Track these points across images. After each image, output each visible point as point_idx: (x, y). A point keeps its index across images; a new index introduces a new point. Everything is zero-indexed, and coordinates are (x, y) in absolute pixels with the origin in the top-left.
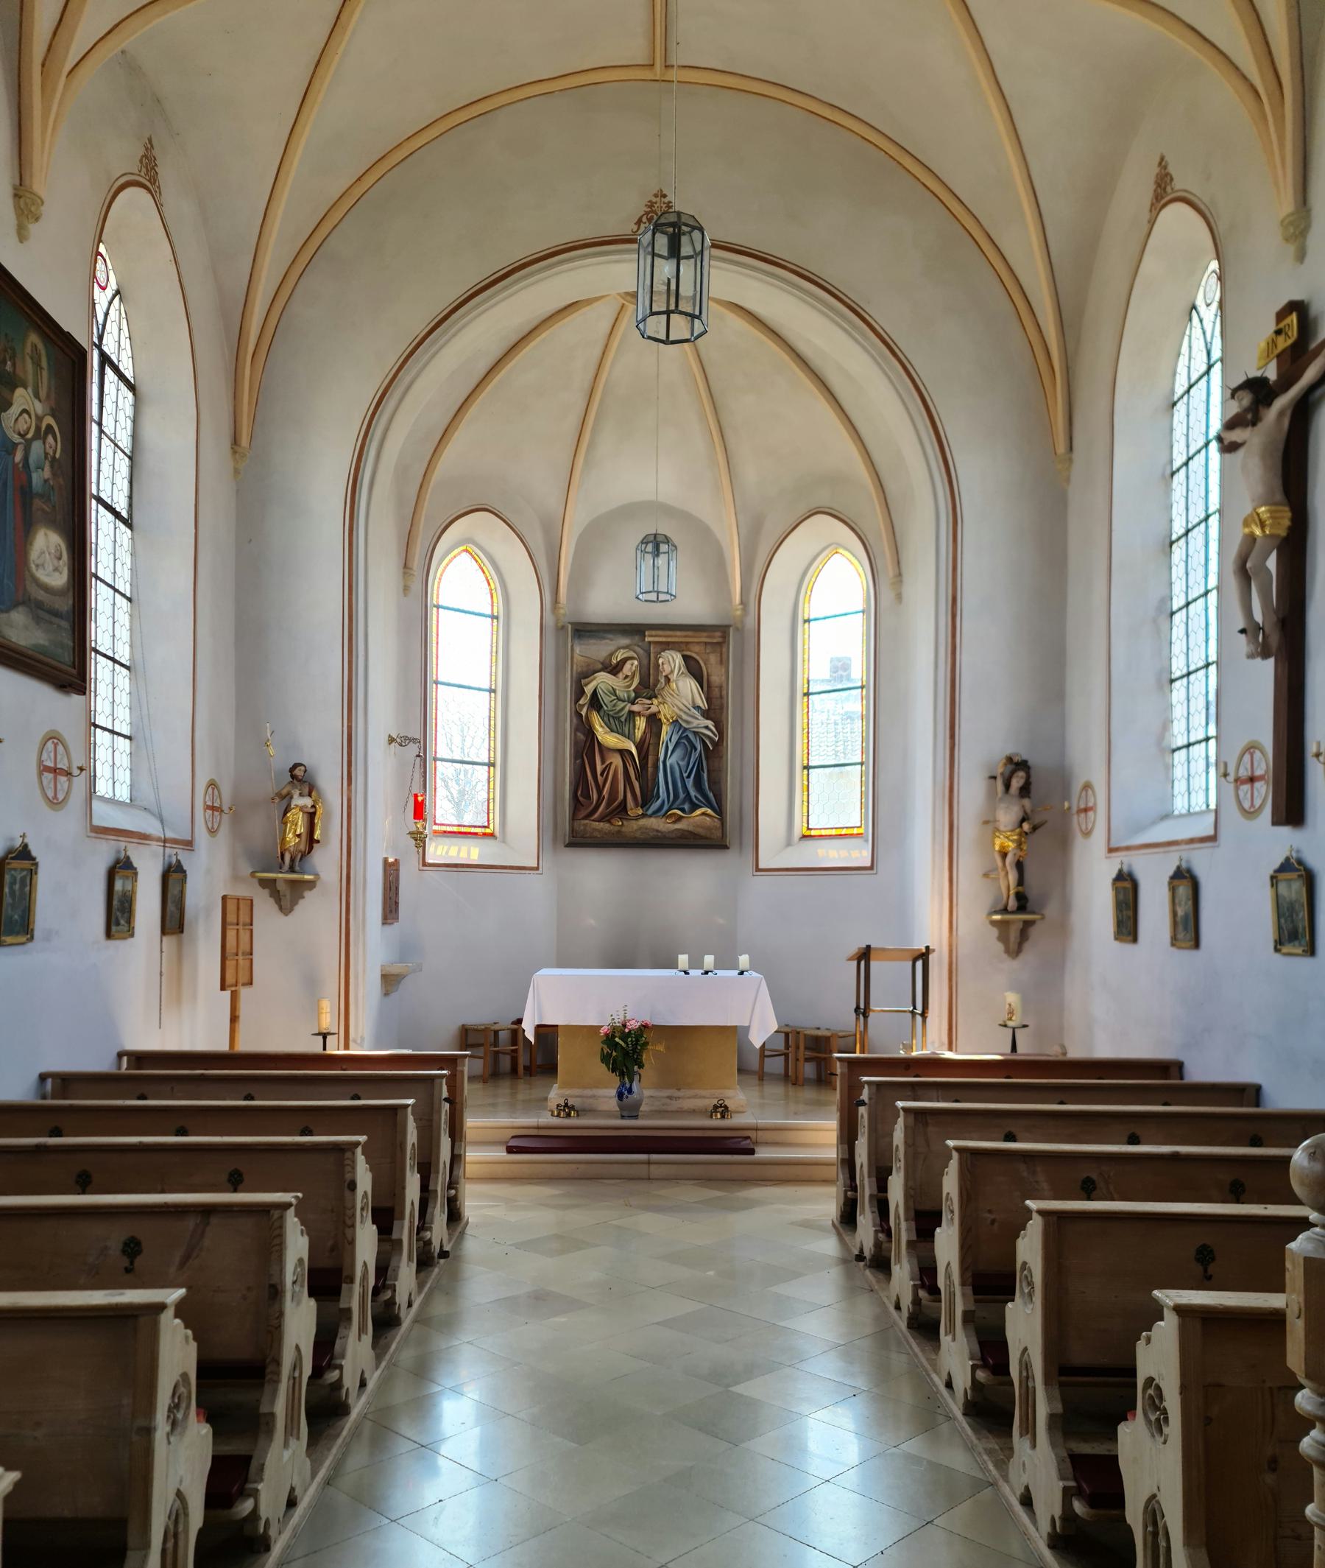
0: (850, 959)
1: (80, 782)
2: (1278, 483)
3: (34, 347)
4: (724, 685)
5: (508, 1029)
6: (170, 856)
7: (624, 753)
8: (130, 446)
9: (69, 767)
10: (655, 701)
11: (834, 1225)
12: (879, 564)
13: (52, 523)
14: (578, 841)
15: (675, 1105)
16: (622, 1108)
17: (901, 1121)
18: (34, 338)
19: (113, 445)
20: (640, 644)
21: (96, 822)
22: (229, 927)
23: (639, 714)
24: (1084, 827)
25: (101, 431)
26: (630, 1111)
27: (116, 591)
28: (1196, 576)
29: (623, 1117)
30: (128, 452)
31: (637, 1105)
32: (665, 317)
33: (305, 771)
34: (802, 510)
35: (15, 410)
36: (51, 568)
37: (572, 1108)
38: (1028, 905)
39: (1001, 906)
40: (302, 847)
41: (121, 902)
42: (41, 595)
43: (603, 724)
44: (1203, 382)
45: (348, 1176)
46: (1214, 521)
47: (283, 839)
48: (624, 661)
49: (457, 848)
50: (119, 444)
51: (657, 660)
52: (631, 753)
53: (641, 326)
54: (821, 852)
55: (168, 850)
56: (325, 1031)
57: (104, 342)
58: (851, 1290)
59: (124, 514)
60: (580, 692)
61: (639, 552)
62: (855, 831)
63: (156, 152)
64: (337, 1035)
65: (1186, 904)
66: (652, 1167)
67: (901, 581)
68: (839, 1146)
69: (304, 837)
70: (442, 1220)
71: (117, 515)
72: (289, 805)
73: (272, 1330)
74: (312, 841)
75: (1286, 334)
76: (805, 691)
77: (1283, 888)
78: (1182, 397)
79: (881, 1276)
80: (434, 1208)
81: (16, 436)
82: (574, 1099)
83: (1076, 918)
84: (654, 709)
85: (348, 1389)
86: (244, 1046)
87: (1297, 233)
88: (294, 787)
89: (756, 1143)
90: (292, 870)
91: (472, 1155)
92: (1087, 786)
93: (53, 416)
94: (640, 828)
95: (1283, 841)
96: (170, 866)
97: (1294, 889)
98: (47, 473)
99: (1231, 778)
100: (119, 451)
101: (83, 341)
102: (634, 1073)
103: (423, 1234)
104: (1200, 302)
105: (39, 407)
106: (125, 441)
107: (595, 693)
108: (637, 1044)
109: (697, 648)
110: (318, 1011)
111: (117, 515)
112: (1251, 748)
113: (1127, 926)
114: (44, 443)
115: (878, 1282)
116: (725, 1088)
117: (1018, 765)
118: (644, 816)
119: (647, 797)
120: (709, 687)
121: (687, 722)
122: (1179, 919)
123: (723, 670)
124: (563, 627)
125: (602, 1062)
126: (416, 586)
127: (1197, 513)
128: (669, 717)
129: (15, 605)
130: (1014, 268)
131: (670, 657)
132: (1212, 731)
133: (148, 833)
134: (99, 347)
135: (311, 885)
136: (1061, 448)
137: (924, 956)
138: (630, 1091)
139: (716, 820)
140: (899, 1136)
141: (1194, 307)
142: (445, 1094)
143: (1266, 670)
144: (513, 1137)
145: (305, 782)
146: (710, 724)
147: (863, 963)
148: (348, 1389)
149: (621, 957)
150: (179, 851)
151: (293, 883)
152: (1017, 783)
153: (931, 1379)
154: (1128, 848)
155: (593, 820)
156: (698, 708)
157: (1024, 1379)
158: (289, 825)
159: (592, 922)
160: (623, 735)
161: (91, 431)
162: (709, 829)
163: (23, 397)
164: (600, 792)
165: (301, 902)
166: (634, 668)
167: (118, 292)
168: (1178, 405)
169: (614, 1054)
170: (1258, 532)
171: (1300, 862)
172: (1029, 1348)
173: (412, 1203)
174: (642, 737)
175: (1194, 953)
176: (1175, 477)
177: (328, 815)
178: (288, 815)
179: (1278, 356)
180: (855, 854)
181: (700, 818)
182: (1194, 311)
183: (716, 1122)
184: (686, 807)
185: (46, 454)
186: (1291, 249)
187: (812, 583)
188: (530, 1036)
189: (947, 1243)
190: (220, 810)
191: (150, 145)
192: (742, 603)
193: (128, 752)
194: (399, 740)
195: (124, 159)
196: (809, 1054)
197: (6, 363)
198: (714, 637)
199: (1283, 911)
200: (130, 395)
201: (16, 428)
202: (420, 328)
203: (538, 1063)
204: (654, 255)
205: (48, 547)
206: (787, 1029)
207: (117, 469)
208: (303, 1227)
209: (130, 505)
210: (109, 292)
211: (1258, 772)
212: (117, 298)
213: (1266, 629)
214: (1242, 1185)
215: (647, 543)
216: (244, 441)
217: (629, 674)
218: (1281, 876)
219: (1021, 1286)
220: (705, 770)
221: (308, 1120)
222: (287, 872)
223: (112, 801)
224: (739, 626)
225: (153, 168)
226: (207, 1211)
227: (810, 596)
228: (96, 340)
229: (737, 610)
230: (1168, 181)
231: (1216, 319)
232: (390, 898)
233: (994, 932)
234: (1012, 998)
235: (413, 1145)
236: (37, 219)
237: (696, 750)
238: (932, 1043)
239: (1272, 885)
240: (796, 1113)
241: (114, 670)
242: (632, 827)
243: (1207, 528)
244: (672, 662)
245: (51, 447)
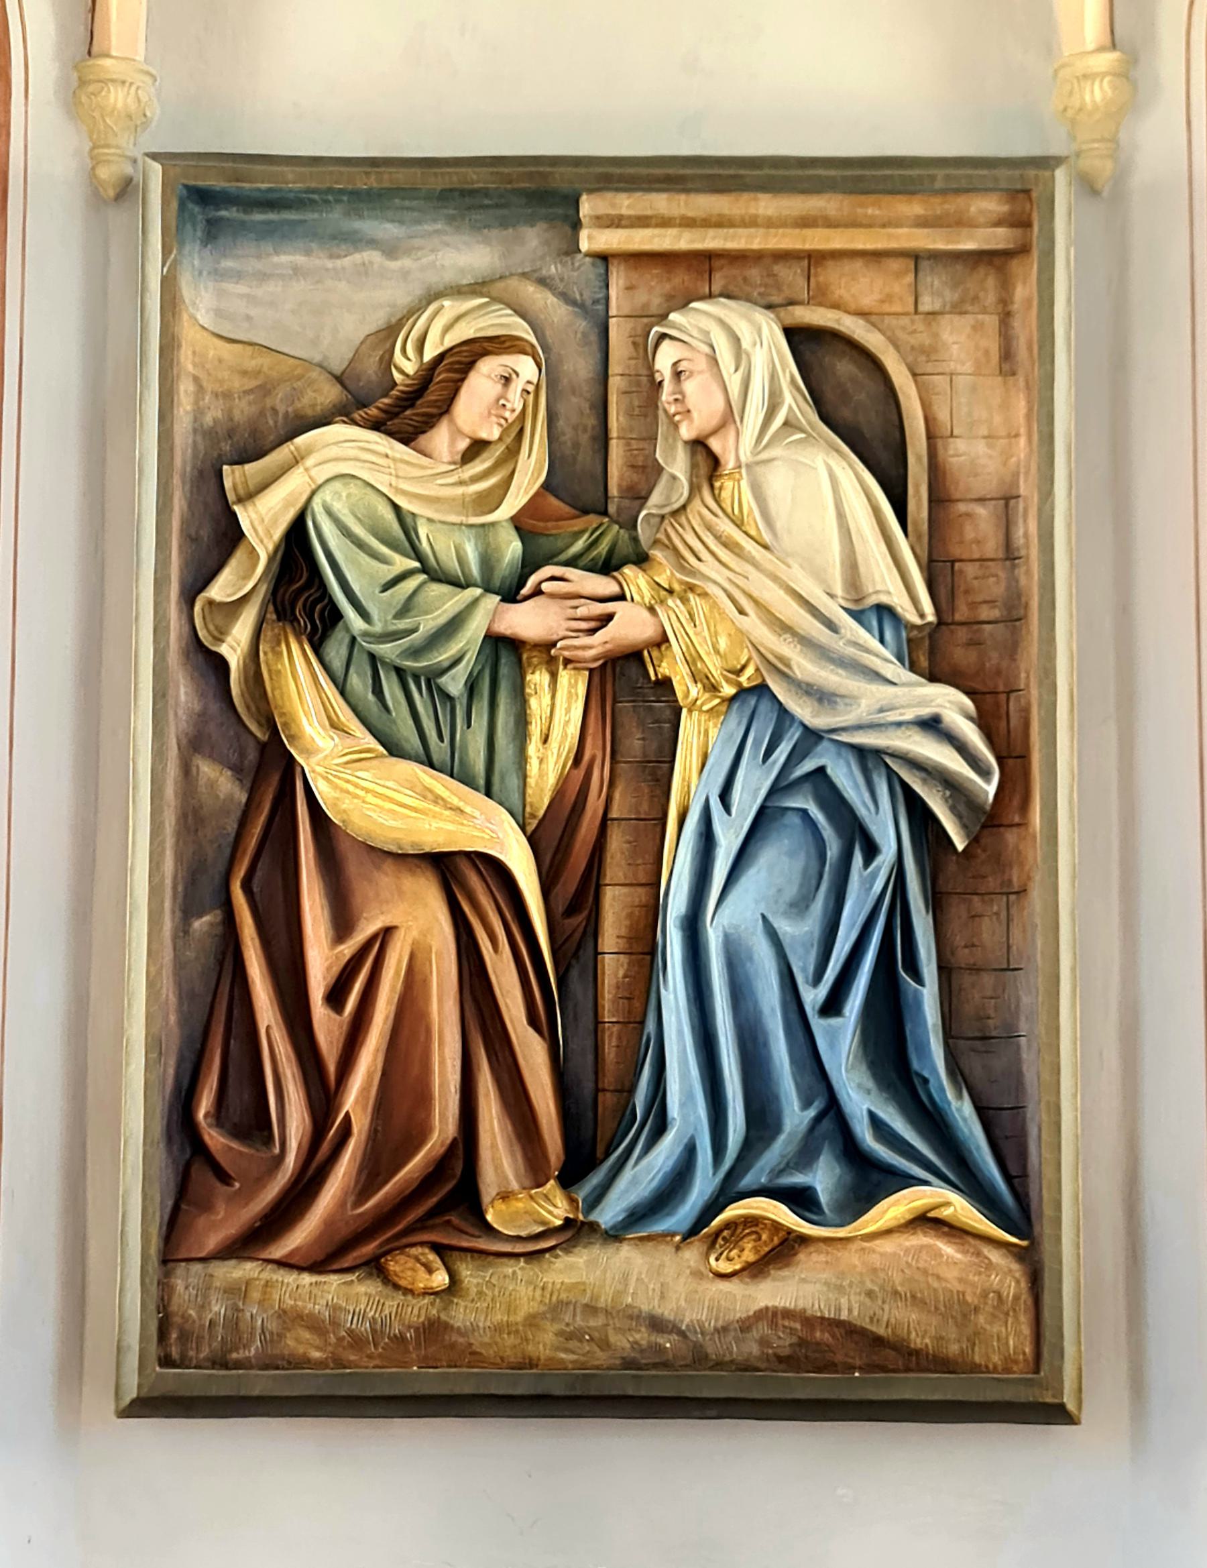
4: (1025, 488)
10: (635, 579)
51: (645, 351)
120: (939, 498)
121: (822, 697)
139: (995, 1256)
155: (282, 1264)
166: (515, 400)
177: (688, 623)
198: (960, 222)
217: (491, 432)
237: (871, 851)
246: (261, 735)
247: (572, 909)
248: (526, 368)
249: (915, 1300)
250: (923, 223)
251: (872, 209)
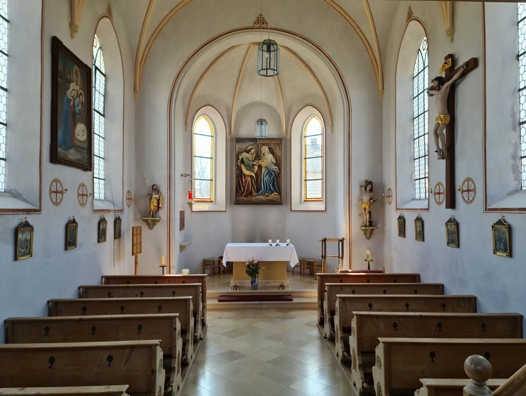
0: (320, 241)
1: (90, 198)
2: (446, 108)
3: (76, 70)
4: (281, 156)
5: (217, 260)
6: (116, 215)
7: (251, 177)
8: (104, 93)
9: (87, 193)
10: (260, 161)
11: (317, 325)
12: (327, 121)
13: (82, 122)
14: (238, 203)
15: (268, 285)
16: (252, 287)
17: (338, 300)
18: (76, 67)
19: (99, 93)
20: (256, 144)
21: (95, 208)
22: (134, 236)
23: (255, 165)
24: (389, 202)
25: (95, 90)
26: (255, 287)
27: (100, 136)
28: (421, 129)
29: (253, 289)
30: (103, 94)
31: (257, 286)
32: (266, 70)
33: (157, 187)
34: (304, 104)
35: (70, 90)
36: (81, 135)
37: (238, 287)
38: (372, 224)
39: (364, 225)
40: (156, 210)
41: (102, 232)
42: (78, 144)
43: (245, 168)
44: (422, 73)
45: (174, 327)
46: (426, 114)
47: (150, 207)
48: (251, 149)
49: (202, 206)
50: (101, 93)
51: (261, 149)
52: (253, 176)
53: (259, 72)
54: (310, 206)
55: (116, 214)
56: (163, 266)
57: (96, 63)
58: (323, 348)
59: (102, 113)
60: (238, 159)
61: (256, 124)
62: (320, 199)
63: (111, 6)
64: (166, 267)
65: (420, 228)
66: (262, 305)
67: (333, 126)
68: (318, 302)
69: (156, 207)
70: (200, 328)
71: (100, 114)
72: (152, 197)
73: (152, 383)
74: (159, 208)
75: (448, 64)
76: (305, 157)
77: (449, 227)
78: (416, 76)
79: (332, 344)
80: (198, 325)
81: (71, 97)
82: (238, 284)
83: (387, 228)
84: (260, 163)
85: (174, 392)
86: (140, 273)
87: (451, 34)
88: (153, 192)
89: (293, 297)
90: (153, 217)
91: (209, 302)
92: (390, 189)
93: (82, 90)
94: (256, 199)
95: (449, 213)
96: (116, 218)
97: (453, 228)
98: (80, 107)
99: (433, 193)
100: (101, 95)
101: (90, 65)
102: (256, 276)
103: (195, 334)
104: (421, 49)
105: (78, 88)
106: (102, 92)
107: (242, 159)
108: (257, 267)
109: (272, 145)
110: (161, 260)
111: (100, 114)
112: (439, 184)
113: (402, 232)
114: (79, 98)
115: (331, 346)
116: (283, 279)
117: (369, 183)
118: (257, 195)
119: (258, 190)
120: (276, 156)
121: (270, 167)
122: (418, 232)
123: (280, 152)
124: (232, 139)
125: (246, 273)
126: (189, 129)
127: (421, 111)
128: (264, 166)
129: (71, 148)
130: (366, 36)
131: (265, 148)
132: (427, 175)
133: (110, 209)
134: (94, 65)
135: (159, 221)
136: (381, 89)
137: (342, 240)
138: (255, 282)
139: (279, 196)
140: (337, 305)
141: (420, 50)
142: (201, 290)
143: (443, 163)
144: (220, 296)
145: (156, 190)
146: (277, 167)
147: (324, 242)
148: (174, 392)
149: (251, 240)
150: (119, 213)
151: (153, 221)
152: (368, 188)
153: (349, 382)
154: (402, 209)
155: (242, 197)
156: (273, 163)
157: (379, 391)
158: (152, 203)
159: (242, 227)
160: (251, 171)
161: (93, 90)
162: (277, 199)
163: (73, 86)
164: (244, 188)
165: (156, 226)
166: (254, 151)
167: (100, 48)
168: (415, 78)
169: (250, 270)
170: (440, 122)
171: (454, 220)
172: (380, 382)
173: (192, 327)
174: (256, 172)
175: (423, 242)
176: (415, 99)
177: (163, 199)
178: (152, 200)
179: (445, 70)
180: (320, 207)
181: (274, 196)
182: (419, 51)
183: (281, 290)
184: (270, 192)
185: (80, 101)
186: (449, 38)
187: (306, 126)
188: (225, 265)
189: (353, 341)
190: (131, 199)
191: (109, 5)
192: (286, 132)
193: (103, 184)
194: (184, 175)
195: (102, 9)
196: (307, 266)
197: (68, 76)
198: (277, 142)
199: (449, 233)
200: (104, 78)
201: (71, 95)
202: (190, 54)
203: (227, 270)
204: (263, 51)
205: (80, 129)
206: (301, 259)
207: (100, 100)
208: (161, 349)
209: (104, 110)
210: (97, 48)
211: (441, 191)
212: (100, 49)
213: (443, 151)
214: (441, 325)
215: (258, 122)
216: (137, 89)
217: (253, 153)
218: (449, 223)
219: (377, 363)
220: (276, 182)
221: (160, 306)
222: (151, 217)
223: (99, 200)
224: (285, 138)
225: (110, 11)
226: (133, 347)
227: (306, 129)
228: (94, 63)
229: (284, 134)
230: (412, 14)
231: (426, 54)
232: (182, 223)
233: (363, 232)
234: (368, 252)
235: (192, 310)
236: (76, 32)
237: (273, 175)
238: (344, 267)
239: (446, 226)
240: (304, 287)
241: (99, 160)
242: (254, 199)
243: (424, 115)
244: (265, 149)
245: (81, 99)
246: (240, 169)
247: (257, 178)
248: (254, 150)
249: (275, 198)
250: (276, 142)
251: (273, 141)
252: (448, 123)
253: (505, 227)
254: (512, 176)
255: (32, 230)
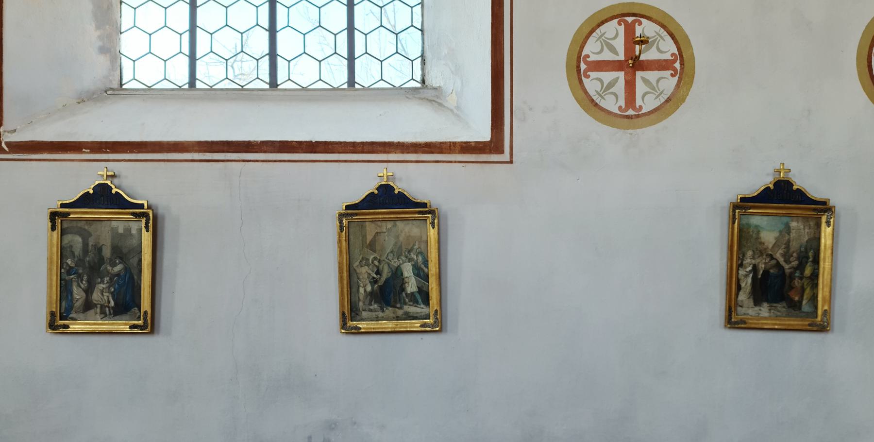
252: (765, 305)
253: (133, 214)
254: (92, 34)
255: (430, 321)
